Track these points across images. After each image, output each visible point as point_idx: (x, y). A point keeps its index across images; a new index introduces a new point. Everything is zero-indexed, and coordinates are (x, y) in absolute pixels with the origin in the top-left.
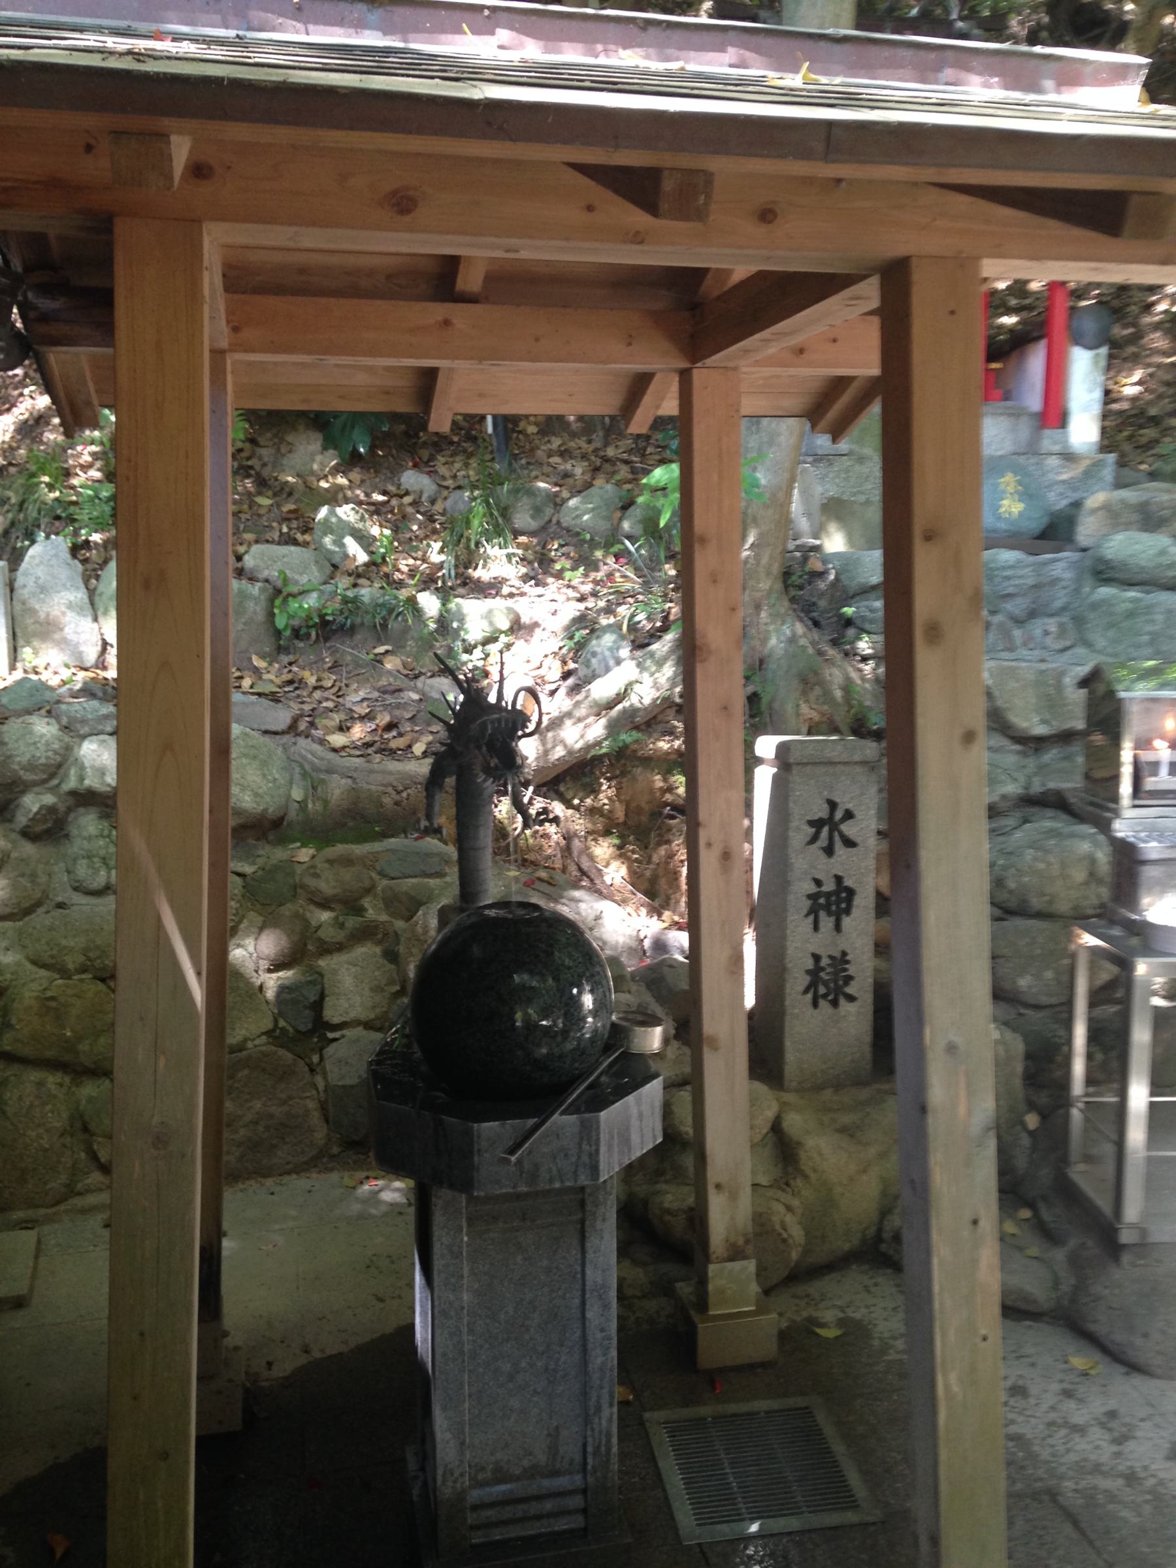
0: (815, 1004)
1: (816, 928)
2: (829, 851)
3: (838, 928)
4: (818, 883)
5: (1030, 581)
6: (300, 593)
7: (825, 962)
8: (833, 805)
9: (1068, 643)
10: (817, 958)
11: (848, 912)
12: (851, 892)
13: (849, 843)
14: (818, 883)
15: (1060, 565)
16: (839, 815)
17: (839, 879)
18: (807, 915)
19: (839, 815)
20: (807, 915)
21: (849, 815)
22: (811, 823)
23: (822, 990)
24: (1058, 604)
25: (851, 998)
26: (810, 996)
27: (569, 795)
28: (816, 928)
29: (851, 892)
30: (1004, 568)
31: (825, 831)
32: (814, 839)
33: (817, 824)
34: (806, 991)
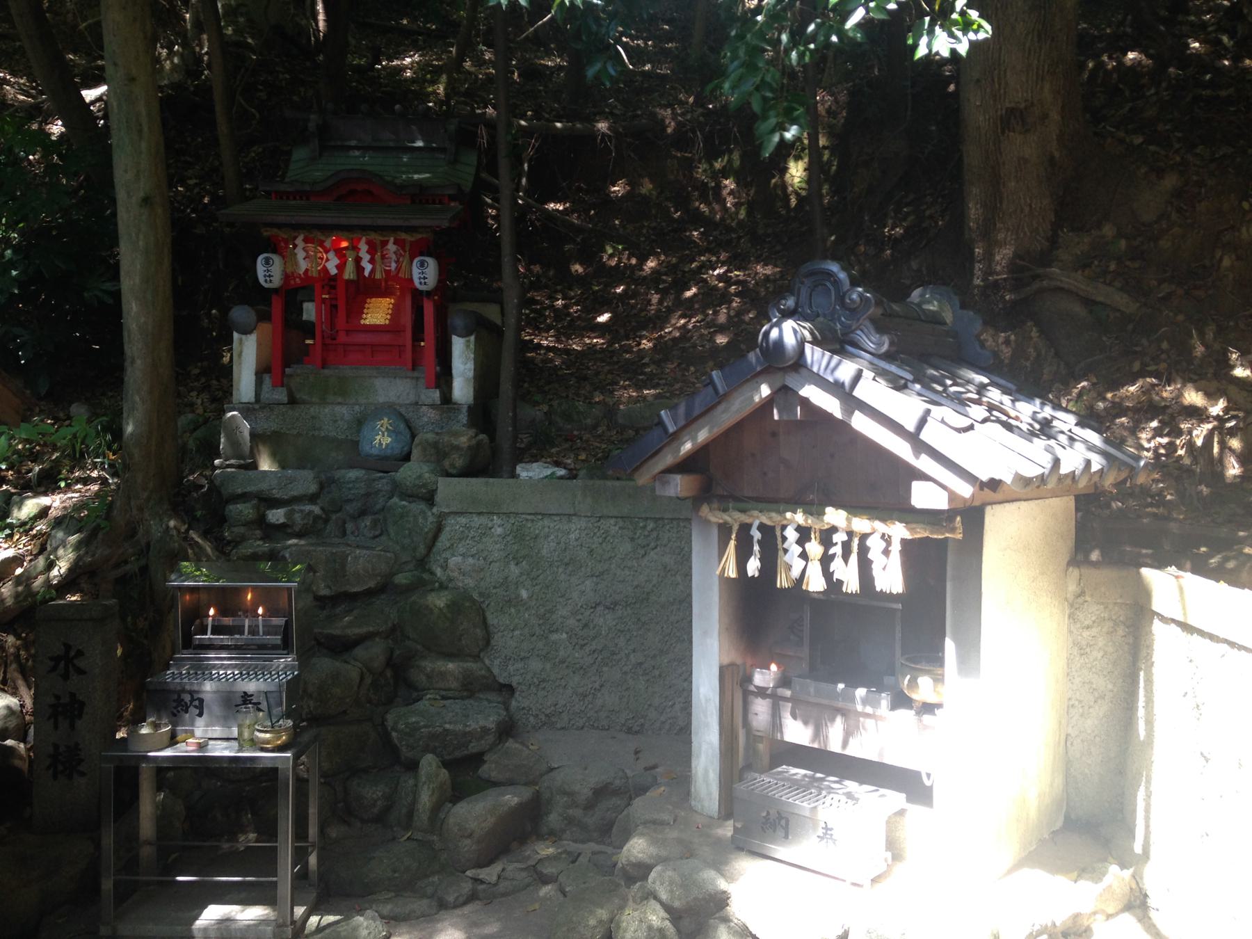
0: (55, 777)
1: (56, 727)
2: (66, 677)
3: (72, 726)
4: (57, 697)
5: (362, 492)
6: (410, 428)
7: (62, 749)
8: (68, 647)
9: (377, 533)
10: (56, 746)
11: (80, 716)
12: (82, 704)
13: (81, 672)
14: (57, 697)
15: (385, 481)
16: (72, 653)
17: (73, 695)
18: (49, 718)
19: (72, 653)
20: (49, 718)
21: (80, 653)
22: (51, 659)
23: (60, 768)
24: (378, 507)
25: (82, 774)
26: (51, 772)
27: (19, 631)
28: (56, 727)
29: (82, 704)
30: (348, 483)
31: (62, 664)
32: (54, 669)
33: (56, 660)
34: (48, 768)
